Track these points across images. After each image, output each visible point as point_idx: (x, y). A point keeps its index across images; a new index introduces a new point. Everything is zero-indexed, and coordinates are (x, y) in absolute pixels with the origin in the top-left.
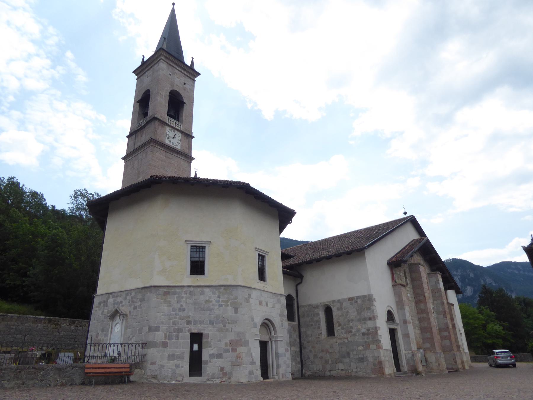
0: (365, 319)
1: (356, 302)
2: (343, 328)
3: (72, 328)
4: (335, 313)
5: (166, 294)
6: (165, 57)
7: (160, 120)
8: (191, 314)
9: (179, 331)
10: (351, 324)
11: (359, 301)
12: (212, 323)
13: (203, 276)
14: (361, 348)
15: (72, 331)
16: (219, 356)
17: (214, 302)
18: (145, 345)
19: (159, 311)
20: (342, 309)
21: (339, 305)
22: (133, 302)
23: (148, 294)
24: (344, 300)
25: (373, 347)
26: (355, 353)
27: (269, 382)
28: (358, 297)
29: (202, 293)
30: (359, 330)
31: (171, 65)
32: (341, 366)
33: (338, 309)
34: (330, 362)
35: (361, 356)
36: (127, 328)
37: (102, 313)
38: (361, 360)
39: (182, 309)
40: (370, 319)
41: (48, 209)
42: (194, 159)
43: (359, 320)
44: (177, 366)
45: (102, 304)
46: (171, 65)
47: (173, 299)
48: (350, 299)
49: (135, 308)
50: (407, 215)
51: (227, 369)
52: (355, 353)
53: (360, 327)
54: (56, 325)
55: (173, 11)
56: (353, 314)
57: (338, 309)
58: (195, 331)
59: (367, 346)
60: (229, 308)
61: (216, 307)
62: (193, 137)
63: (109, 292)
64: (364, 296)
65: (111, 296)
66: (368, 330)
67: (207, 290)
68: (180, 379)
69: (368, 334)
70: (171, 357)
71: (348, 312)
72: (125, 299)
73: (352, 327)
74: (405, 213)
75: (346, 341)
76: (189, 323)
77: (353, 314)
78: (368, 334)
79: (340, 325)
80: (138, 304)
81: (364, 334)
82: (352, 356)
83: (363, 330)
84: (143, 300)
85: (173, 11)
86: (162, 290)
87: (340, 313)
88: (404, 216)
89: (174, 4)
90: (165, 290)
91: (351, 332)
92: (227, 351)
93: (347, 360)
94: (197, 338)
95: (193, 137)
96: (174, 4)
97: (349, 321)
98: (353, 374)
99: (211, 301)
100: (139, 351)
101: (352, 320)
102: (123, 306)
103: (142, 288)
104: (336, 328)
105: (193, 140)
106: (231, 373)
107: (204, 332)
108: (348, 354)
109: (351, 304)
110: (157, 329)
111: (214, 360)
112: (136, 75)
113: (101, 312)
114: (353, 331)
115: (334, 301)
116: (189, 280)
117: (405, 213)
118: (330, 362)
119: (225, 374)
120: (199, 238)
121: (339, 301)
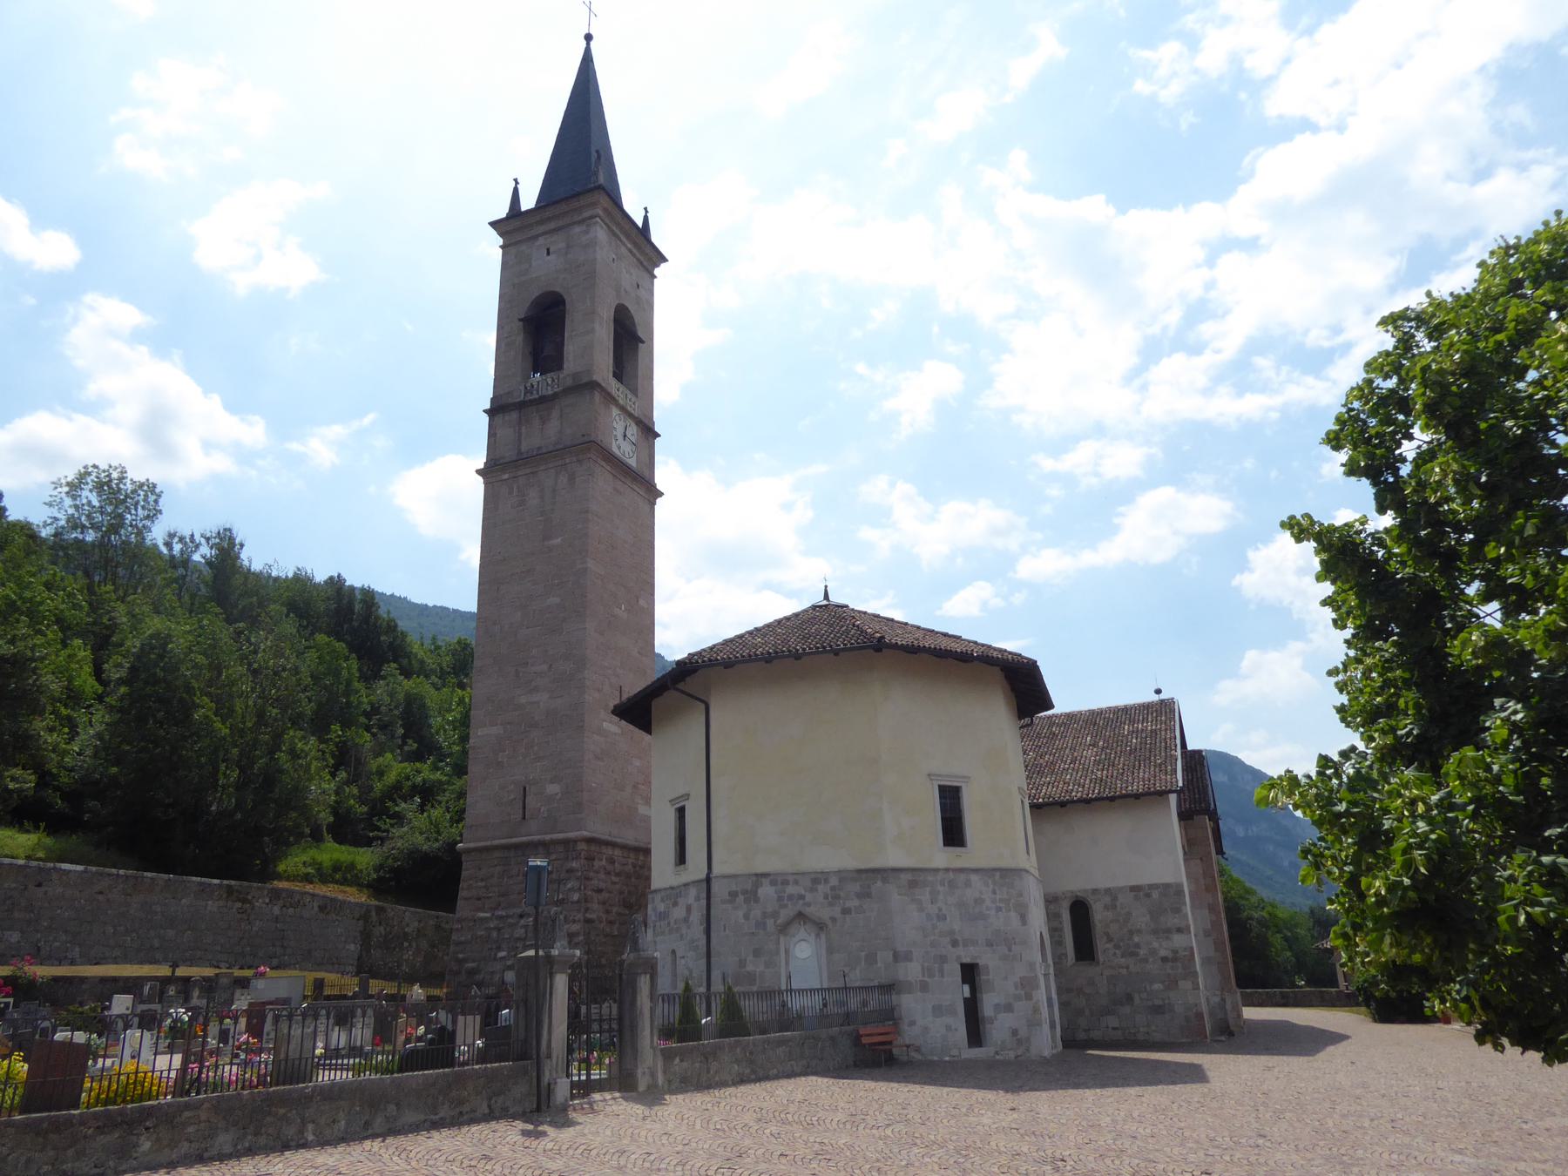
0: (1168, 931)
1: (1148, 895)
2: (1117, 947)
3: (276, 910)
4: (1099, 915)
5: (913, 884)
6: (605, 210)
7: (603, 390)
8: (956, 927)
9: (943, 959)
10: (1136, 939)
11: (1155, 895)
12: (990, 944)
13: (958, 850)
14: (1157, 986)
15: (277, 920)
16: (1009, 1008)
17: (988, 903)
18: (889, 988)
19: (907, 920)
20: (1114, 907)
21: (1107, 899)
22: (837, 897)
23: (879, 884)
24: (1121, 889)
25: (1185, 985)
26: (1144, 995)
27: (1147, 1061)
28: (1151, 886)
29: (968, 884)
30: (1153, 952)
31: (614, 234)
32: (1112, 1021)
33: (1106, 907)
34: (1087, 1012)
35: (1158, 1002)
36: (830, 951)
37: (746, 917)
38: (1158, 1010)
39: (942, 917)
40: (1179, 930)
41: (185, 562)
42: (661, 494)
43: (1155, 932)
44: (949, 1028)
45: (741, 898)
46: (614, 234)
47: (924, 895)
48: (1135, 889)
49: (846, 911)
50: (1162, 696)
51: (1023, 1033)
52: (1144, 995)
53: (1156, 945)
54: (244, 901)
55: (587, 61)
56: (1140, 917)
57: (1106, 907)
58: (967, 960)
59: (1172, 983)
60: (1013, 914)
61: (993, 912)
62: (658, 435)
63: (760, 871)
64: (1167, 886)
65: (766, 881)
66: (1175, 952)
67: (974, 878)
68: (955, 1052)
69: (1175, 960)
70: (938, 1011)
71: (1129, 914)
72: (813, 890)
73: (1138, 946)
74: (1158, 692)
75: (1124, 971)
76: (955, 943)
77: (1140, 917)
78: (1175, 960)
79: (1110, 940)
80: (853, 903)
81: (1165, 959)
82: (1137, 1001)
83: (1163, 953)
84: (865, 895)
85: (587, 61)
86: (904, 877)
87: (1110, 915)
88: (1156, 698)
89: (588, 38)
90: (909, 876)
91: (1137, 954)
92: (1018, 998)
93: (1127, 1010)
94: (970, 973)
95: (658, 435)
96: (588, 38)
97: (1131, 933)
98: (1140, 1037)
99: (983, 901)
100: (874, 1001)
101: (1139, 931)
102: (809, 905)
103: (859, 871)
104: (1101, 945)
105: (657, 441)
106: (1028, 1039)
107: (981, 962)
108: (1129, 998)
109: (1136, 898)
110: (908, 957)
111: (1001, 1016)
112: (501, 235)
113: (740, 914)
114: (1142, 952)
115: (1095, 891)
116: (942, 857)
117: (1158, 692)
118: (1087, 1012)
119: (1019, 1042)
120: (952, 769)
121: (1108, 891)
